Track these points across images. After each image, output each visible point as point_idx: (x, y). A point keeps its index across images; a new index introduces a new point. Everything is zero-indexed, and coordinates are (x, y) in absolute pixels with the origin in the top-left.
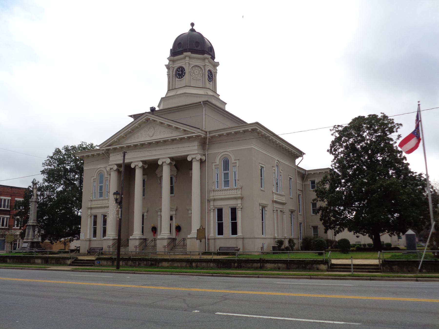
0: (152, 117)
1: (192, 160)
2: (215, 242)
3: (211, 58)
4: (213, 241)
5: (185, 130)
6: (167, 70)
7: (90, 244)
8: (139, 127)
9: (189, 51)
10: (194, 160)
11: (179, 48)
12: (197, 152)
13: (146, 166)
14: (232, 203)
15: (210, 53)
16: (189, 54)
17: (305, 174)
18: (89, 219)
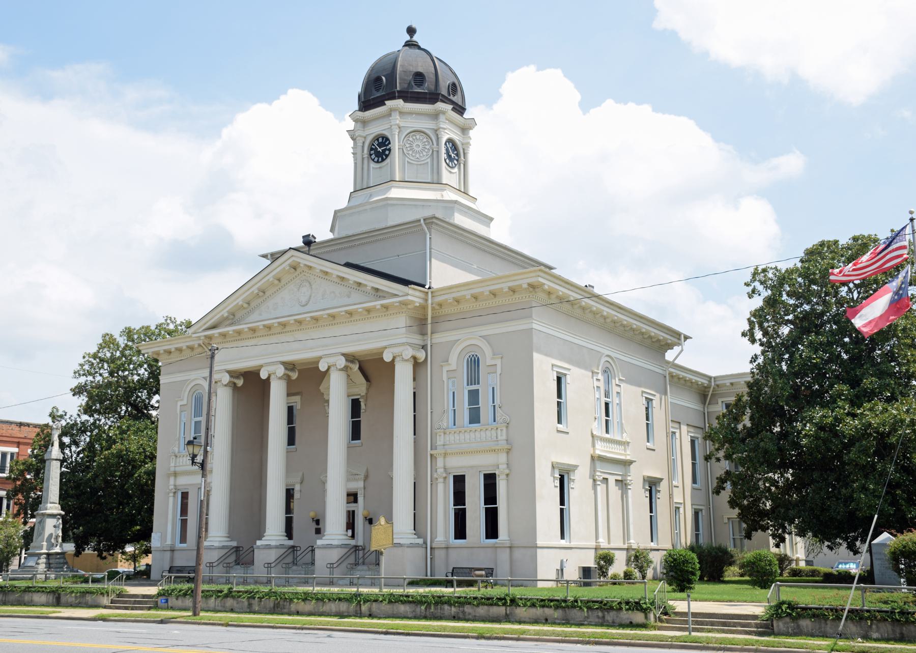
0: (304, 259)
1: (393, 360)
2: (447, 555)
3: (454, 109)
4: (443, 552)
5: (377, 290)
6: (351, 143)
7: (172, 559)
8: (276, 282)
9: (399, 98)
10: (397, 359)
11: (378, 90)
12: (404, 340)
13: (240, 382)
15: (451, 97)
16: (399, 103)
17: (709, 387)
18: (171, 499)
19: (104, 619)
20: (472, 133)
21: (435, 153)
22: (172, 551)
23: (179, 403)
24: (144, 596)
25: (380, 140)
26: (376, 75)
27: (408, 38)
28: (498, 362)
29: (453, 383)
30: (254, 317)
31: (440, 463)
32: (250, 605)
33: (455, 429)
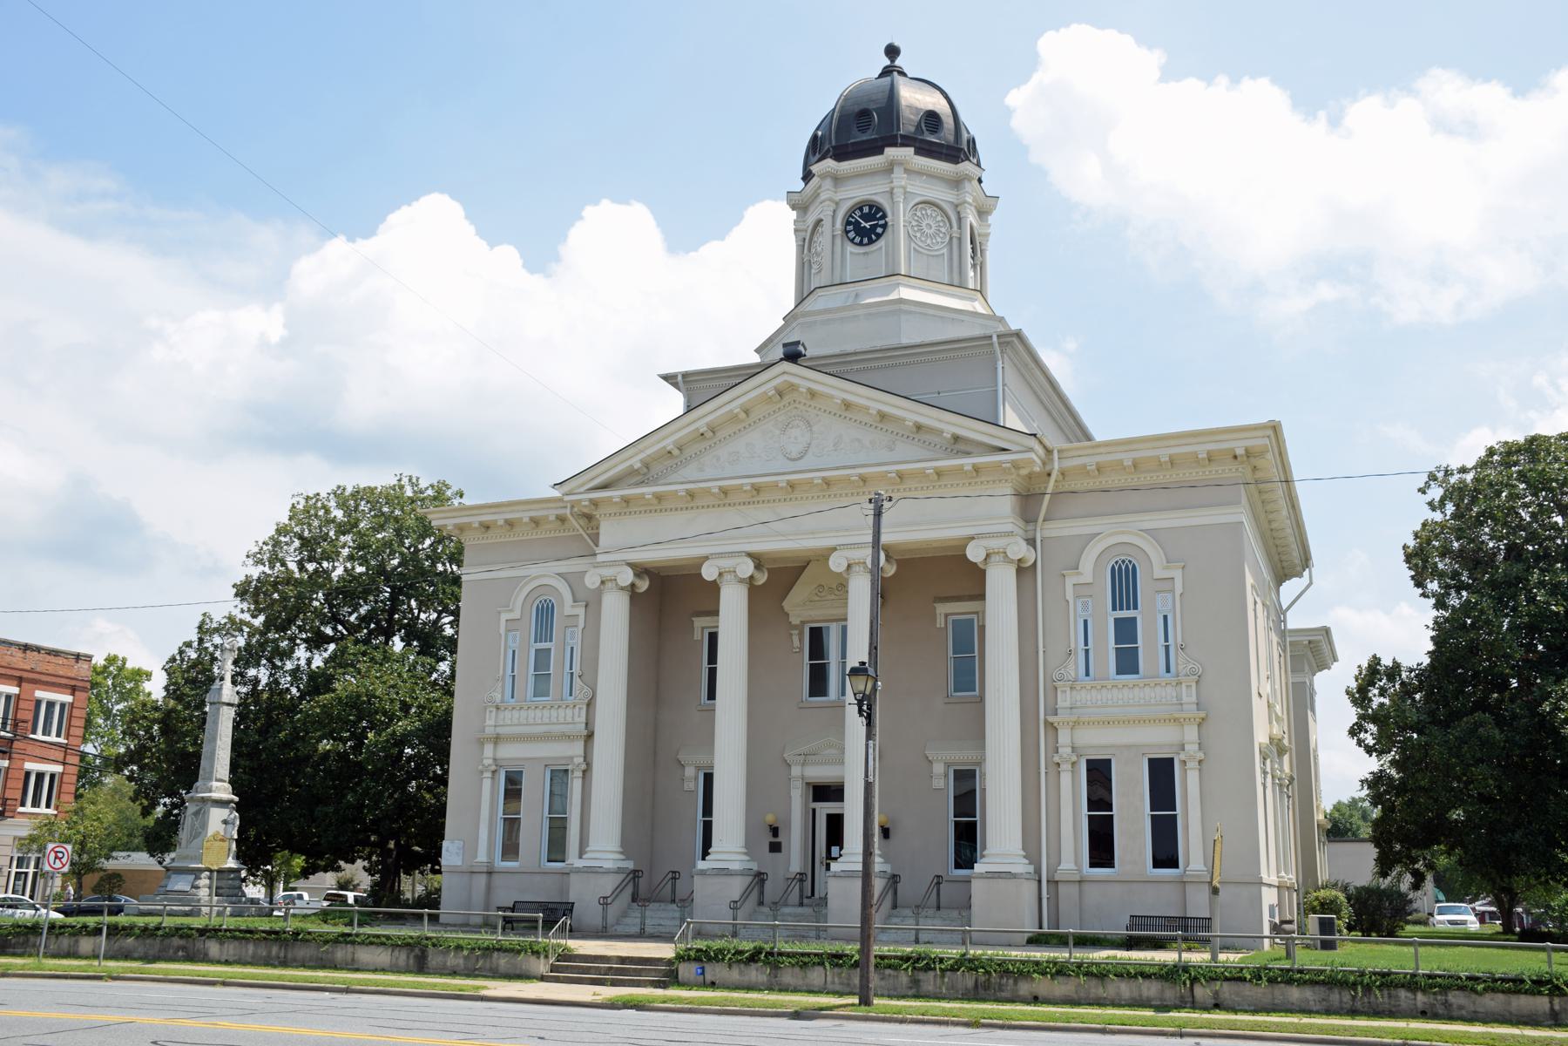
4: (1074, 889)
8: (743, 415)
11: (863, 131)
13: (643, 585)
14: (1159, 740)
18: (487, 784)
19: (639, 1006)
20: (991, 219)
21: (955, 241)
22: (490, 873)
23: (504, 617)
24: (623, 960)
25: (866, 210)
26: (865, 106)
27: (888, 62)
28: (1178, 575)
29: (1085, 605)
30: (690, 472)
31: (1064, 737)
32: (915, 982)
33: (1088, 682)
